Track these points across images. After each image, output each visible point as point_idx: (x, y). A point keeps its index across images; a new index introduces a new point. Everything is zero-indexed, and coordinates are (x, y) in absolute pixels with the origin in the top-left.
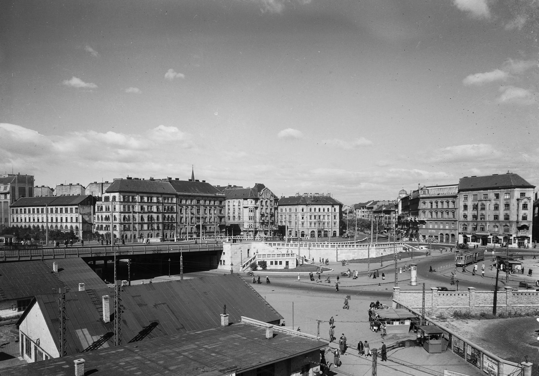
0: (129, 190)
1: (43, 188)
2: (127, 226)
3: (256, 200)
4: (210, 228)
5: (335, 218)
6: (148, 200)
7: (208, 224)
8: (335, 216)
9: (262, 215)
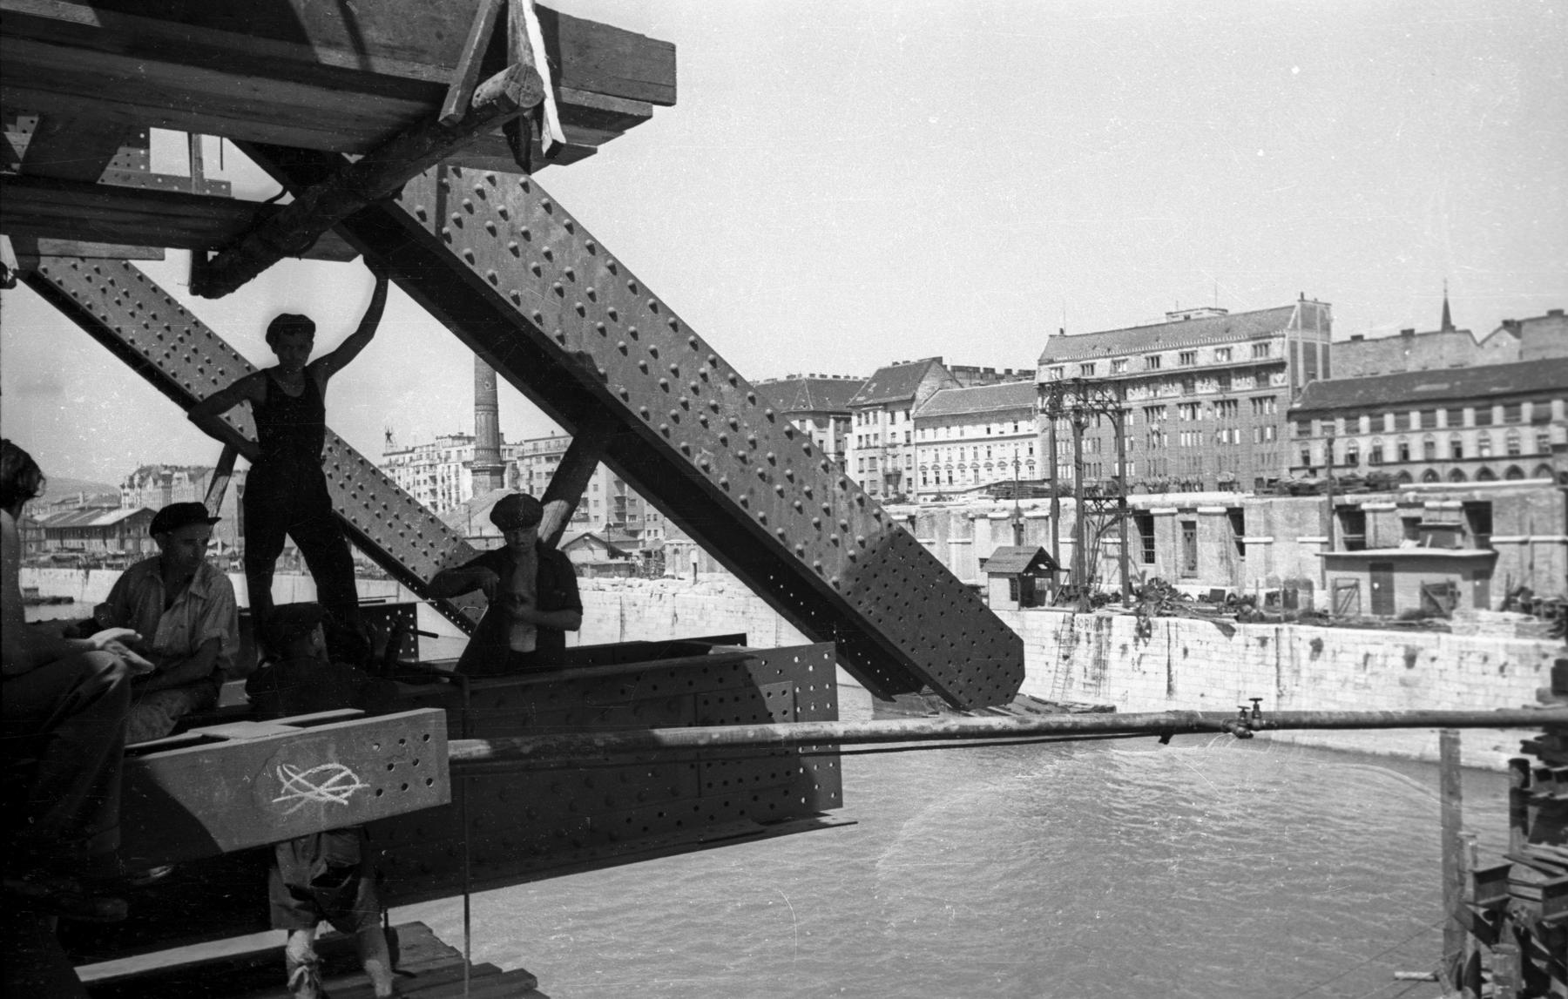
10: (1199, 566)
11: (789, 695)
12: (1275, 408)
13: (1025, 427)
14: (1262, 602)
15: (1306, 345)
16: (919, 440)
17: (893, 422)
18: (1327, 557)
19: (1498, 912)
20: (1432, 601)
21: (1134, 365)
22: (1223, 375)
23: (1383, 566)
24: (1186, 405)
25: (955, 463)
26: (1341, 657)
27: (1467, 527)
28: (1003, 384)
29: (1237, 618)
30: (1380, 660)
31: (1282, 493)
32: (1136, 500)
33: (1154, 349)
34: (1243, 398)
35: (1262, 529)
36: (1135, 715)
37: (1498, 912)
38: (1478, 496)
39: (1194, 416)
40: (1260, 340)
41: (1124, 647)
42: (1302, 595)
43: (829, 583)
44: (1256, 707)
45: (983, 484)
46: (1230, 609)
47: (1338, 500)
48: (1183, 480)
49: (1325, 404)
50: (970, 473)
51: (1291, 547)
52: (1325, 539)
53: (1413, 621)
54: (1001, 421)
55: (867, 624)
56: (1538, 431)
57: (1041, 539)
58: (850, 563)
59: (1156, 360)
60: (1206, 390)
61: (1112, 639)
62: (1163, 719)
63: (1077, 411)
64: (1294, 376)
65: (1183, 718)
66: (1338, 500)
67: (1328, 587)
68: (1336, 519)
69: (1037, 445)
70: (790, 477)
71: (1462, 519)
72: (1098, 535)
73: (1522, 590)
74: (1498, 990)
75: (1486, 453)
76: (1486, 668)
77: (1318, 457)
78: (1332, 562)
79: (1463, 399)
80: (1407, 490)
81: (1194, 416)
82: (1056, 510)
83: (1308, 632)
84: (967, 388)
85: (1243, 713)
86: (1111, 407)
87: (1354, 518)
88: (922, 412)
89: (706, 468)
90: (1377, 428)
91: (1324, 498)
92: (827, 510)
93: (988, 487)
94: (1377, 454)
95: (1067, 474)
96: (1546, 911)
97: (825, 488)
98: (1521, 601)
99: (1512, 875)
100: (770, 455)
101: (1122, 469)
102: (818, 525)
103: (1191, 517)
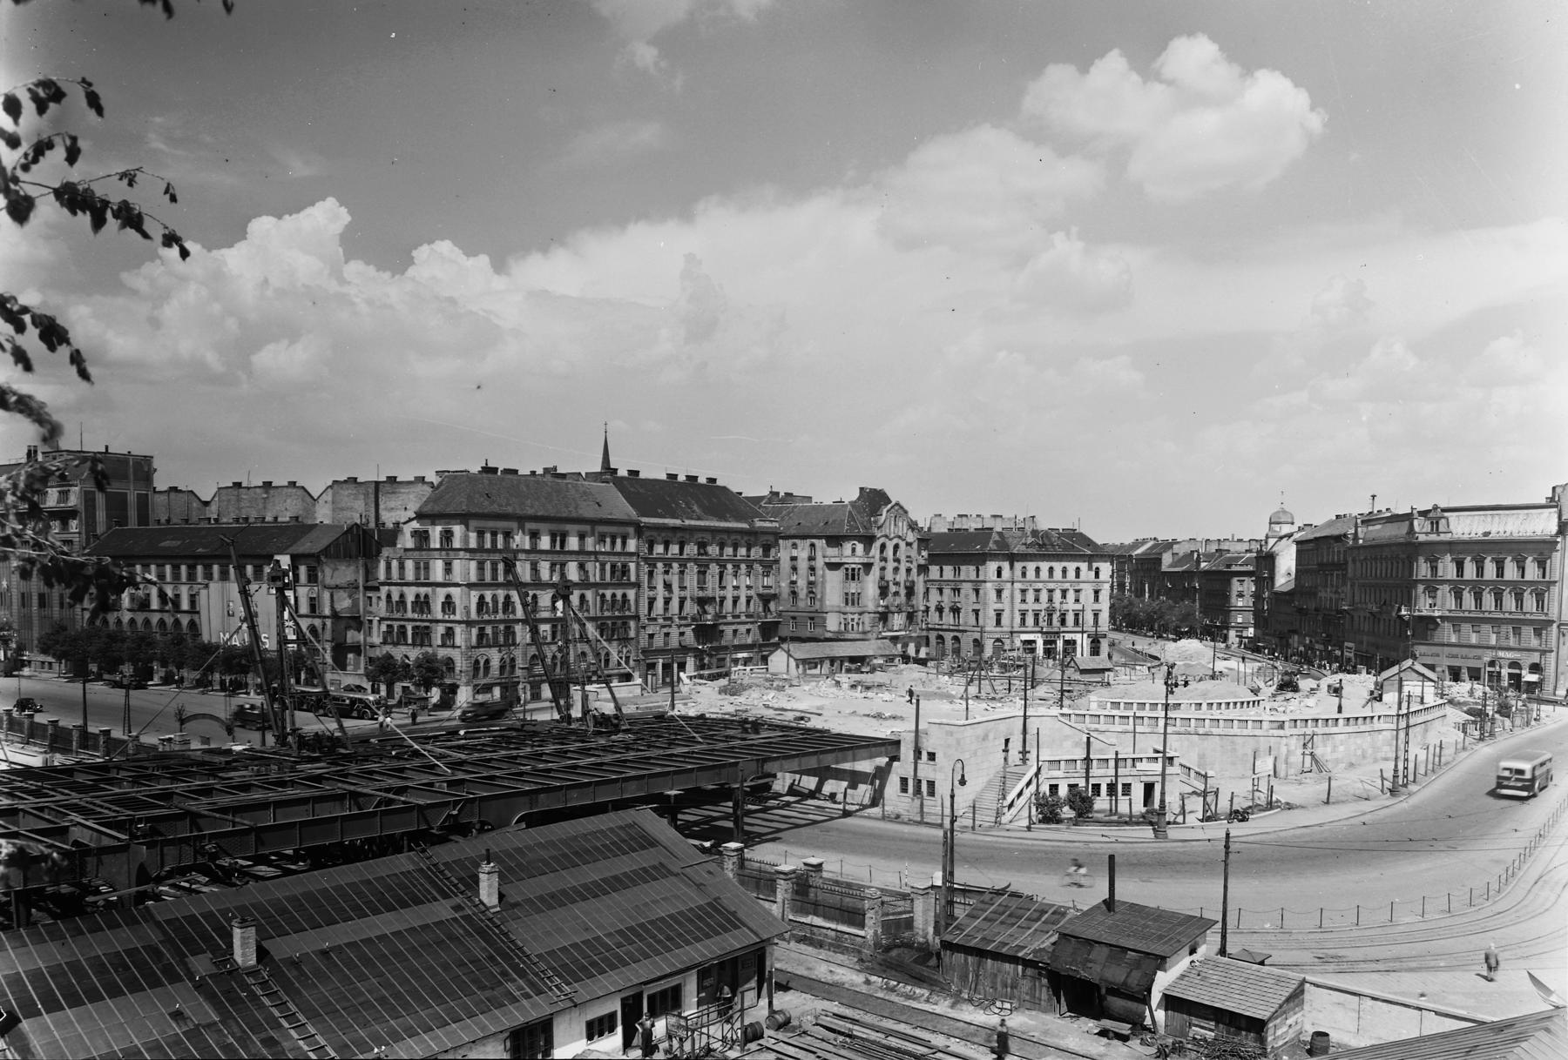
0: (495, 508)
1: (173, 495)
2: (489, 630)
3: (868, 540)
4: (735, 631)
5: (1097, 599)
6: (553, 542)
7: (730, 619)
8: (1097, 592)
9: (884, 591)
79: (149, 557)
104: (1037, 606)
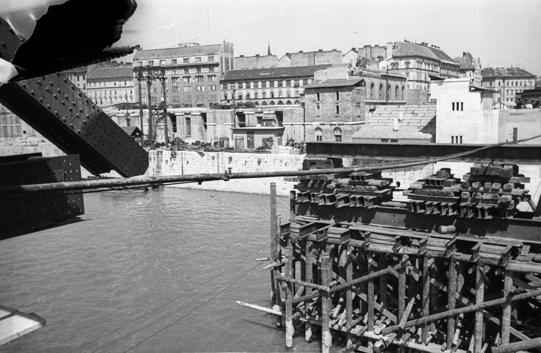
10: (192, 133)
11: (63, 175)
12: (216, 78)
13: (129, 83)
14: (213, 145)
15: (225, 58)
16: (89, 87)
17: (78, 80)
18: (234, 130)
19: (287, 237)
20: (265, 143)
21: (167, 62)
22: (198, 67)
23: (251, 132)
24: (186, 77)
25: (103, 96)
26: (238, 162)
27: (276, 119)
28: (120, 67)
29: (205, 150)
30: (250, 163)
31: (219, 108)
32: (170, 110)
33: (175, 57)
34: (205, 75)
35: (213, 120)
36: (190, 175)
37: (287, 237)
38: (279, 109)
39: (188, 81)
40: (211, 55)
41: (167, 161)
42: (225, 142)
43: (76, 132)
44: (230, 171)
45: (113, 104)
46: (202, 147)
47: (237, 110)
48: (185, 104)
49: (233, 78)
50: (109, 100)
51: (222, 126)
52: (233, 124)
53: (260, 150)
54: (120, 81)
55: (91, 148)
56: (296, 89)
57: (136, 124)
58: (84, 125)
59: (175, 61)
60: (193, 72)
61: (163, 159)
62: (200, 176)
63: (149, 78)
64: (222, 69)
65: (206, 176)
66: (237, 110)
67: (234, 139)
68: (236, 117)
69: (133, 90)
70: (59, 91)
71: (275, 117)
72: (157, 122)
73: (292, 139)
74: (287, 260)
75: (281, 96)
76: (281, 164)
77: (229, 97)
78: (235, 131)
79: (274, 78)
80: (258, 108)
81: (188, 81)
82: (141, 114)
83: (228, 154)
84: (106, 68)
85: (226, 173)
86: (160, 76)
87: (242, 116)
88: (89, 77)
89: (25, 87)
90: (248, 87)
91: (232, 110)
92: (74, 105)
93: (116, 105)
94: (248, 95)
95: (145, 101)
96: (300, 236)
97: (73, 96)
98: (291, 143)
99: (291, 226)
100: (51, 82)
101: (165, 100)
102: (71, 110)
103: (189, 116)
104: (512, 96)
